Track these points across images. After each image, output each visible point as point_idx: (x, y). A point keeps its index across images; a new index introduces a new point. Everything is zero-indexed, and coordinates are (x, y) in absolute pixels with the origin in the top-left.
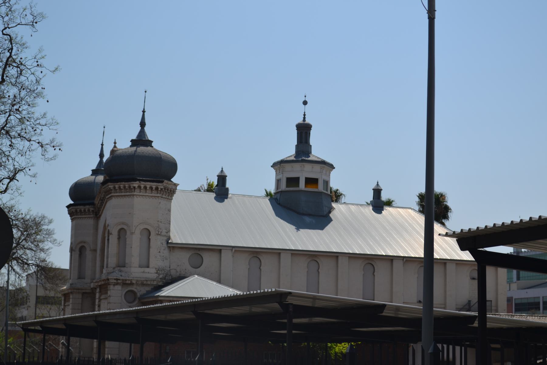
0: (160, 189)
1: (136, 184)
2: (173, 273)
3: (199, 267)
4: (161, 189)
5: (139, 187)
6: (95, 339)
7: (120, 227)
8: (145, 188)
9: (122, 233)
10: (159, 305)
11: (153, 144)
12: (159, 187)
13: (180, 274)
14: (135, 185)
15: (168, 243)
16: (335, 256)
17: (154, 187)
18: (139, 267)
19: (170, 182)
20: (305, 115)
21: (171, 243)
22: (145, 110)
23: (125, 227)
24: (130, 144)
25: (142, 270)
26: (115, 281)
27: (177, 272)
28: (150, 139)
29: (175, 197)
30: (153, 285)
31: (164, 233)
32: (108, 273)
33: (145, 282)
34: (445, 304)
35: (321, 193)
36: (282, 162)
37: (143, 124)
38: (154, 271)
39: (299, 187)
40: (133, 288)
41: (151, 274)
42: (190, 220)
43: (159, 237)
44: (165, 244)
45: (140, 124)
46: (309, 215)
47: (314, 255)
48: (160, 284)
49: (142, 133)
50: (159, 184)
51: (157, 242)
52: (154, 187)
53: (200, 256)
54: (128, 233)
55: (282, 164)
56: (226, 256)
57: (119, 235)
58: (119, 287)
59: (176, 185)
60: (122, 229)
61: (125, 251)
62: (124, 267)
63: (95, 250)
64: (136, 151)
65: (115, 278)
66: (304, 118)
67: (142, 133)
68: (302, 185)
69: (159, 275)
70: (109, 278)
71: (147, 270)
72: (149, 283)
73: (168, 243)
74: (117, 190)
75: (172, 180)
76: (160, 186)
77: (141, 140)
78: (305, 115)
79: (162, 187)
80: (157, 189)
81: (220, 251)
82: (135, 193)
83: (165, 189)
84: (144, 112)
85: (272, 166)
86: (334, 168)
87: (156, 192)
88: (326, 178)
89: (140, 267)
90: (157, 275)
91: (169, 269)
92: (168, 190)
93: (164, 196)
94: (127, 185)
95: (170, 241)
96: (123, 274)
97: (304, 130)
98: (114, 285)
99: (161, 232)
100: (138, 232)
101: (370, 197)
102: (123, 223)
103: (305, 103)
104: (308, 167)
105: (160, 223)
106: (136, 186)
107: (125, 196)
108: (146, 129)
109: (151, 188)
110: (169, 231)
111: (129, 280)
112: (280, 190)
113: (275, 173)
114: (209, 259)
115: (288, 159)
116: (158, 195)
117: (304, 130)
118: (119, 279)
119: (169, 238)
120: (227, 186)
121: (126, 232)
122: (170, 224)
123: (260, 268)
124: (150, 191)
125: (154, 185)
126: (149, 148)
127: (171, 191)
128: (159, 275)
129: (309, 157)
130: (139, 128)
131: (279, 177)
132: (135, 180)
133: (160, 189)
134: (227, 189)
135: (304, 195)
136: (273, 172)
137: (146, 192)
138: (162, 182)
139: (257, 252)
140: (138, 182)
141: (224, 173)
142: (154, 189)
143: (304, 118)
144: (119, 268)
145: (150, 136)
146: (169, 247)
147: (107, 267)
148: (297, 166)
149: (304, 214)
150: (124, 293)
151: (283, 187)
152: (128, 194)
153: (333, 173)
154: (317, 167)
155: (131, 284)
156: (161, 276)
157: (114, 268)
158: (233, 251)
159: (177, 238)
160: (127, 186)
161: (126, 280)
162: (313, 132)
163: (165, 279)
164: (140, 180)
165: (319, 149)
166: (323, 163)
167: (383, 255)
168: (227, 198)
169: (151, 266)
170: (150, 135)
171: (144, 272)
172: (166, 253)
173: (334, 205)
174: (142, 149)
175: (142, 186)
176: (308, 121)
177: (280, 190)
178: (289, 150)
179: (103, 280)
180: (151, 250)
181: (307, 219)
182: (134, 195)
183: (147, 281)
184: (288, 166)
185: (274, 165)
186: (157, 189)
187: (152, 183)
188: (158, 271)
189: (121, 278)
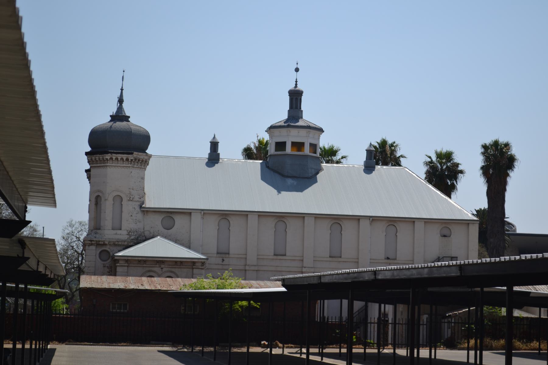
1: (108, 156)
4: (132, 160)
5: (111, 159)
6: (504, 307)
7: (97, 194)
8: (117, 159)
10: (507, 258)
14: (107, 157)
15: (141, 207)
16: (302, 216)
17: (125, 158)
18: (113, 229)
19: (144, 154)
20: (296, 82)
21: (144, 208)
23: (100, 194)
24: (110, 118)
25: (115, 232)
26: (90, 242)
27: (150, 233)
28: (127, 114)
29: (148, 168)
30: (124, 245)
31: (137, 198)
33: (117, 243)
34: (413, 261)
35: (307, 156)
38: (125, 232)
40: (107, 248)
41: (123, 235)
42: (161, 188)
43: (130, 203)
44: (138, 209)
47: (281, 216)
49: (120, 108)
50: (130, 156)
51: (129, 207)
52: (125, 158)
53: (170, 220)
54: (103, 200)
58: (93, 248)
59: (150, 156)
62: (100, 229)
64: (111, 127)
66: (296, 84)
67: (120, 108)
69: (130, 236)
71: (119, 232)
72: (120, 243)
73: (141, 207)
74: (97, 161)
75: (147, 151)
77: (119, 116)
78: (296, 82)
79: (132, 158)
80: (127, 160)
81: (190, 214)
84: (122, 90)
86: (323, 132)
87: (122, 162)
88: (313, 142)
93: (135, 166)
94: (101, 157)
97: (295, 96)
98: (89, 246)
99: (133, 198)
100: (110, 199)
103: (297, 70)
104: (294, 132)
105: (132, 190)
107: (100, 166)
108: (124, 105)
115: (277, 125)
117: (295, 96)
119: (143, 203)
120: (219, 152)
124: (122, 162)
125: (125, 156)
126: (125, 123)
129: (298, 121)
132: (108, 153)
134: (219, 154)
135: (290, 157)
138: (132, 154)
139: (226, 214)
140: (110, 154)
143: (296, 84)
146: (144, 211)
149: (288, 177)
150: (98, 252)
152: (103, 165)
154: (303, 132)
155: (105, 244)
156: (132, 237)
159: (150, 203)
160: (101, 158)
161: (99, 241)
164: (111, 153)
165: (310, 114)
168: (217, 163)
170: (127, 110)
171: (116, 234)
172: (140, 216)
173: (324, 165)
174: (119, 125)
176: (300, 87)
181: (290, 181)
182: (107, 166)
184: (276, 131)
186: (127, 160)
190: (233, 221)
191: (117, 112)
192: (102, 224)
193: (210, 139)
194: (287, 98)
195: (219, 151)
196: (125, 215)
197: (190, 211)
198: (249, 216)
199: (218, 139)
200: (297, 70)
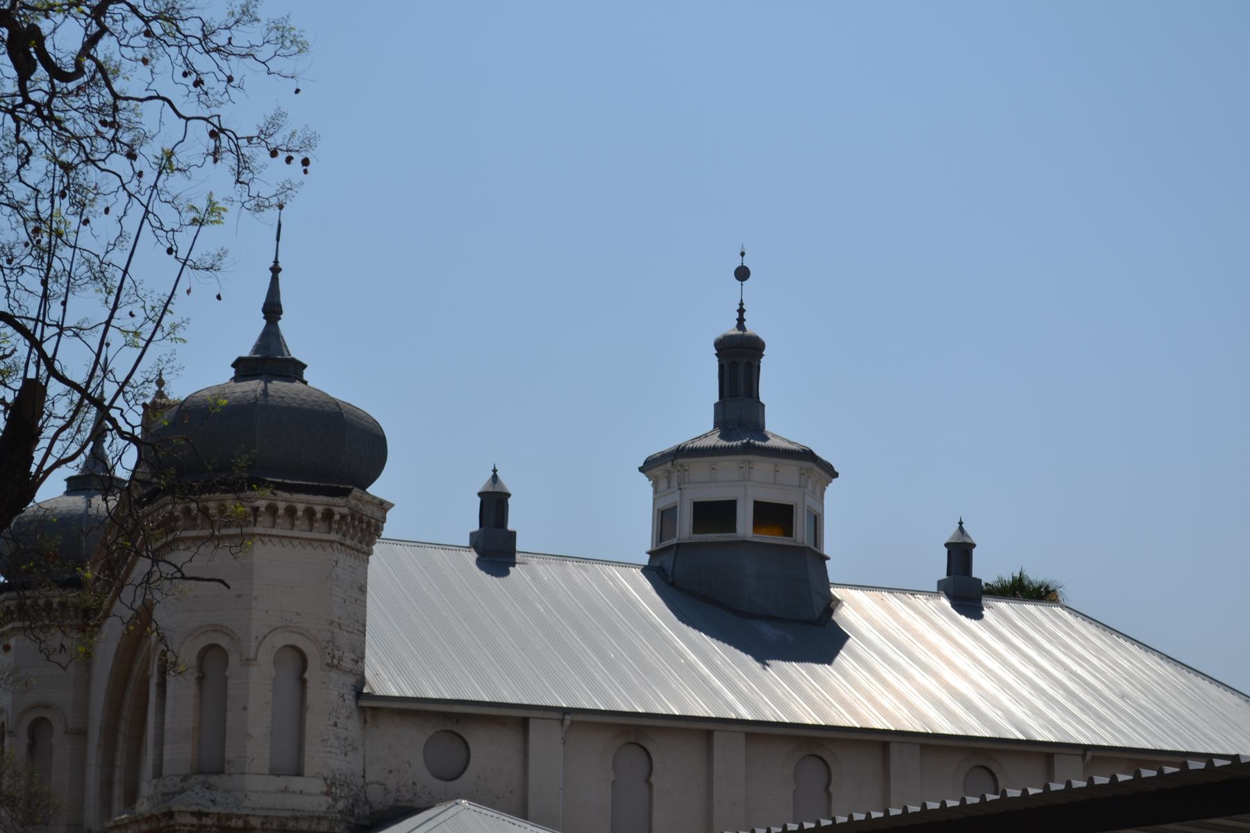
0: (337, 517)
2: (375, 794)
3: (459, 776)
4: (343, 517)
5: (272, 510)
7: (33, 715)
8: (291, 512)
9: (213, 664)
11: (306, 375)
12: (336, 509)
13: (396, 800)
14: (258, 503)
15: (359, 694)
17: (319, 510)
20: (741, 311)
21: (371, 696)
22: (280, 265)
23: (223, 641)
24: (231, 372)
25: (281, 782)
26: (194, 821)
31: (347, 664)
32: (165, 794)
36: (681, 453)
37: (272, 310)
38: (317, 786)
39: (734, 530)
43: (334, 675)
44: (350, 698)
45: (264, 310)
46: (771, 619)
48: (368, 823)
50: (337, 500)
51: (325, 692)
52: (319, 510)
54: (234, 661)
55: (680, 461)
56: (543, 740)
57: (201, 668)
59: (384, 506)
60: (44, 719)
61: (225, 720)
62: (221, 772)
63: (83, 733)
65: (195, 809)
66: (741, 320)
68: (745, 525)
69: (336, 800)
70: (174, 809)
71: (296, 783)
73: (359, 694)
76: (340, 506)
77: (269, 360)
78: (741, 311)
79: (345, 511)
80: (328, 515)
81: (524, 723)
82: (258, 530)
83: (353, 516)
84: (276, 270)
85: (641, 469)
86: (836, 475)
89: (275, 772)
90: (329, 799)
91: (360, 781)
92: (361, 521)
93: (348, 542)
95: (365, 691)
96: (218, 796)
97: (739, 358)
99: (340, 659)
100: (265, 658)
101: (939, 568)
102: (217, 629)
103: (742, 274)
104: (762, 467)
105: (337, 630)
106: (262, 504)
109: (310, 513)
110: (360, 658)
111: (239, 817)
112: (666, 543)
113: (651, 490)
114: (488, 751)
115: (698, 444)
116: (333, 536)
117: (739, 358)
118: (207, 815)
119: (362, 681)
120: (510, 527)
121: (227, 656)
122: (364, 633)
123: (648, 781)
125: (319, 503)
127: (366, 526)
128: (336, 800)
130: (259, 324)
131: (666, 503)
133: (337, 517)
134: (513, 535)
136: (644, 486)
137: (292, 527)
138: (346, 493)
140: (268, 493)
141: (502, 485)
142: (319, 515)
143: (741, 320)
144: (202, 778)
145: (296, 349)
147: (158, 773)
148: (729, 465)
151: (684, 529)
153: (833, 491)
154: (790, 470)
156: (341, 805)
157: (185, 778)
158: (567, 722)
159: (386, 678)
161: (229, 817)
162: (767, 365)
163: (351, 813)
165: (784, 421)
166: (807, 455)
167: (1018, 741)
168: (513, 564)
169: (308, 770)
171: (286, 791)
172: (353, 727)
175: (282, 506)
176: (752, 328)
177: (674, 541)
178: (693, 416)
179: (147, 819)
180: (310, 718)
181: (769, 631)
182: (252, 535)
183: (296, 818)
184: (698, 468)
185: (648, 467)
186: (328, 515)
187: (311, 498)
188: (332, 785)
189: (213, 810)
190: (662, 751)
191: (258, 348)
192: (229, 754)
193: (481, 482)
194: (711, 365)
195: (514, 522)
196: (316, 722)
197: (524, 714)
198: (716, 736)
199: (508, 482)
200: (742, 274)
